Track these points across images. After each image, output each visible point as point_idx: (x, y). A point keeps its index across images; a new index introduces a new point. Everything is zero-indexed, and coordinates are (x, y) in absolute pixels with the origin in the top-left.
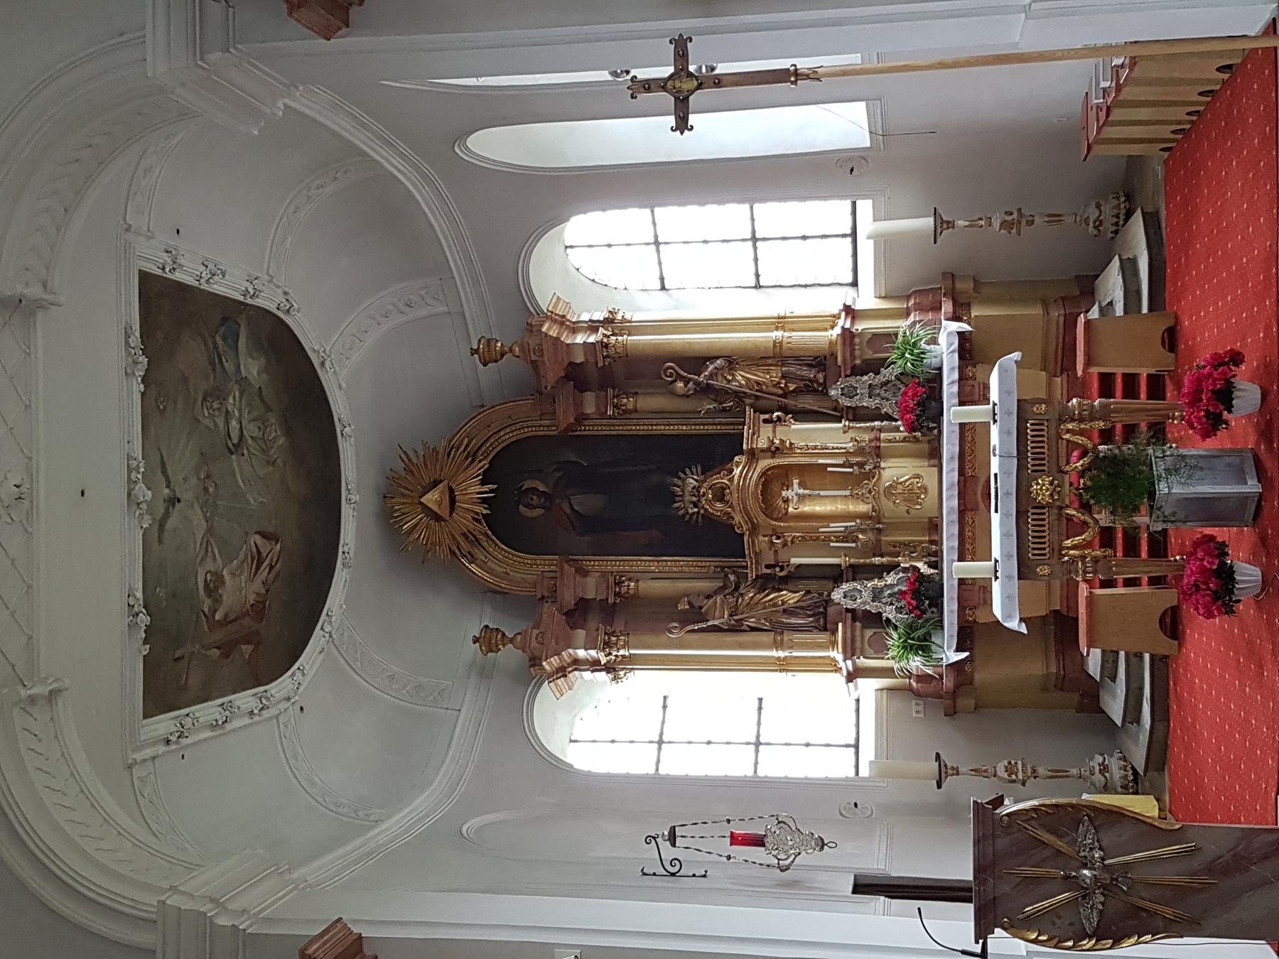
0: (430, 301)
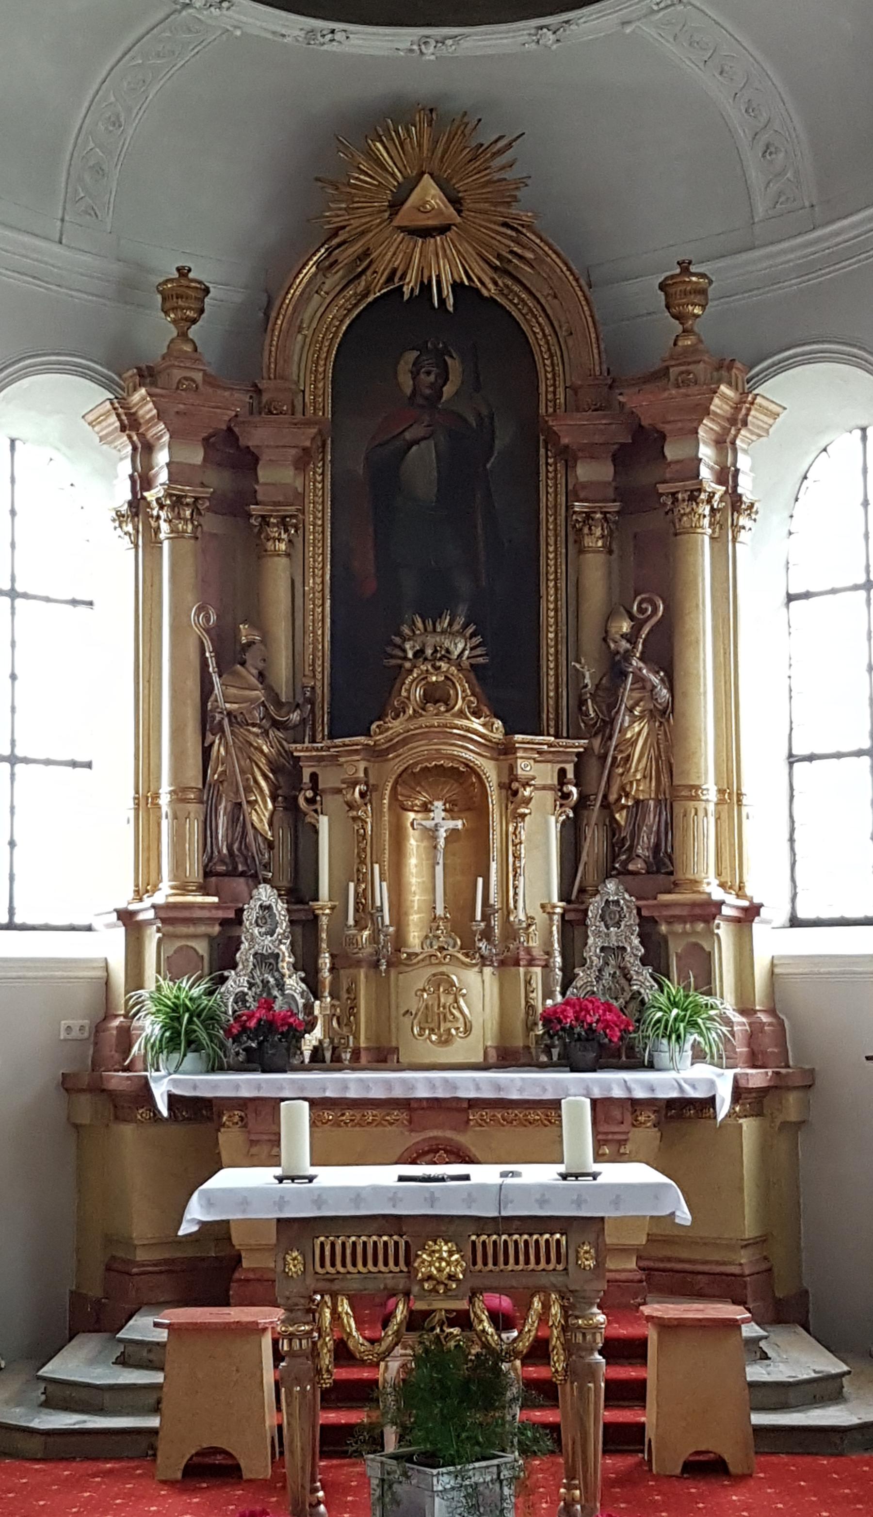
0: (774, 188)
